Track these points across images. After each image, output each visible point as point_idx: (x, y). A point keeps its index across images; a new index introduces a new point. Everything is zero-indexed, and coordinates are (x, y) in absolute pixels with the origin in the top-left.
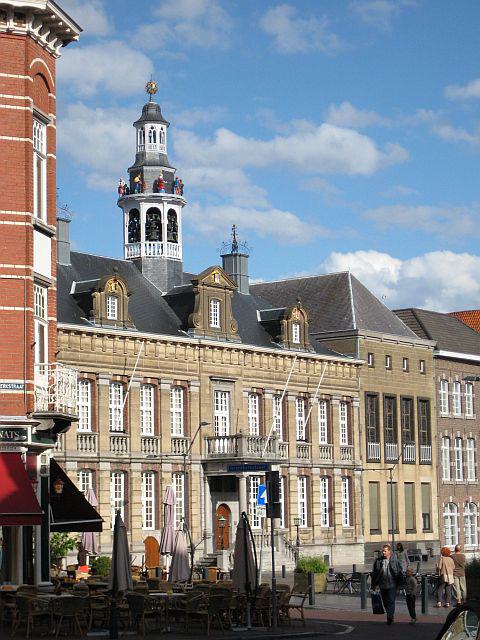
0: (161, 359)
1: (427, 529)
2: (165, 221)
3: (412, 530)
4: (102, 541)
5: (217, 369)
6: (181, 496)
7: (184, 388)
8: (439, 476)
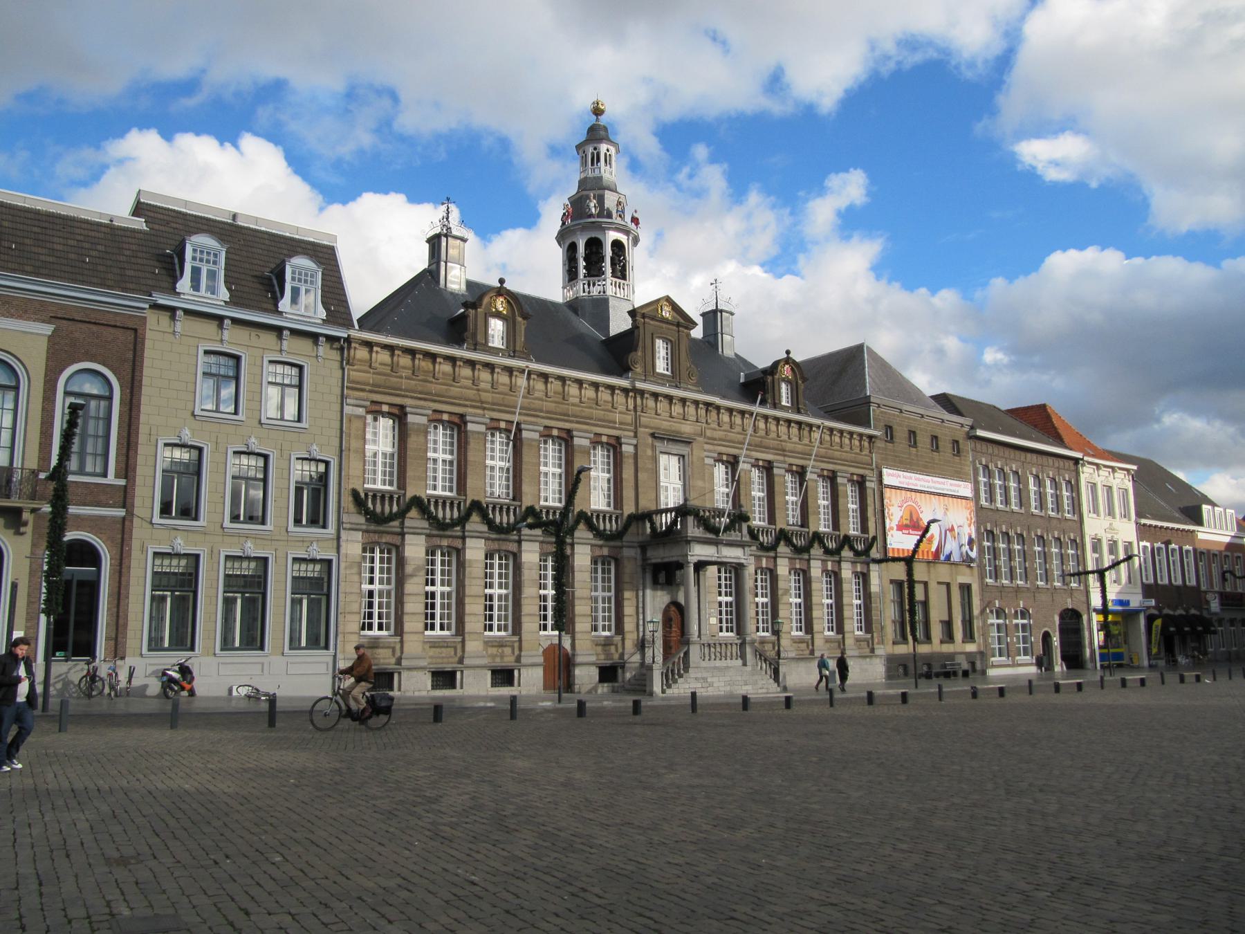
0: (573, 405)
1: (969, 636)
2: (608, 252)
3: (949, 636)
4: (467, 648)
5: (666, 425)
6: (609, 591)
7: (614, 446)
8: (982, 577)
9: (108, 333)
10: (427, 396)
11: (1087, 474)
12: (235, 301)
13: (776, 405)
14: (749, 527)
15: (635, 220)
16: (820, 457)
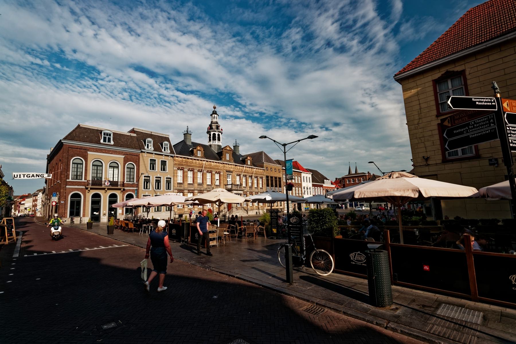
2: (217, 136)
9: (133, 156)
10: (188, 166)
11: (303, 175)
12: (154, 150)
13: (247, 165)
14: (417, 31)
15: (222, 130)
16: (255, 174)
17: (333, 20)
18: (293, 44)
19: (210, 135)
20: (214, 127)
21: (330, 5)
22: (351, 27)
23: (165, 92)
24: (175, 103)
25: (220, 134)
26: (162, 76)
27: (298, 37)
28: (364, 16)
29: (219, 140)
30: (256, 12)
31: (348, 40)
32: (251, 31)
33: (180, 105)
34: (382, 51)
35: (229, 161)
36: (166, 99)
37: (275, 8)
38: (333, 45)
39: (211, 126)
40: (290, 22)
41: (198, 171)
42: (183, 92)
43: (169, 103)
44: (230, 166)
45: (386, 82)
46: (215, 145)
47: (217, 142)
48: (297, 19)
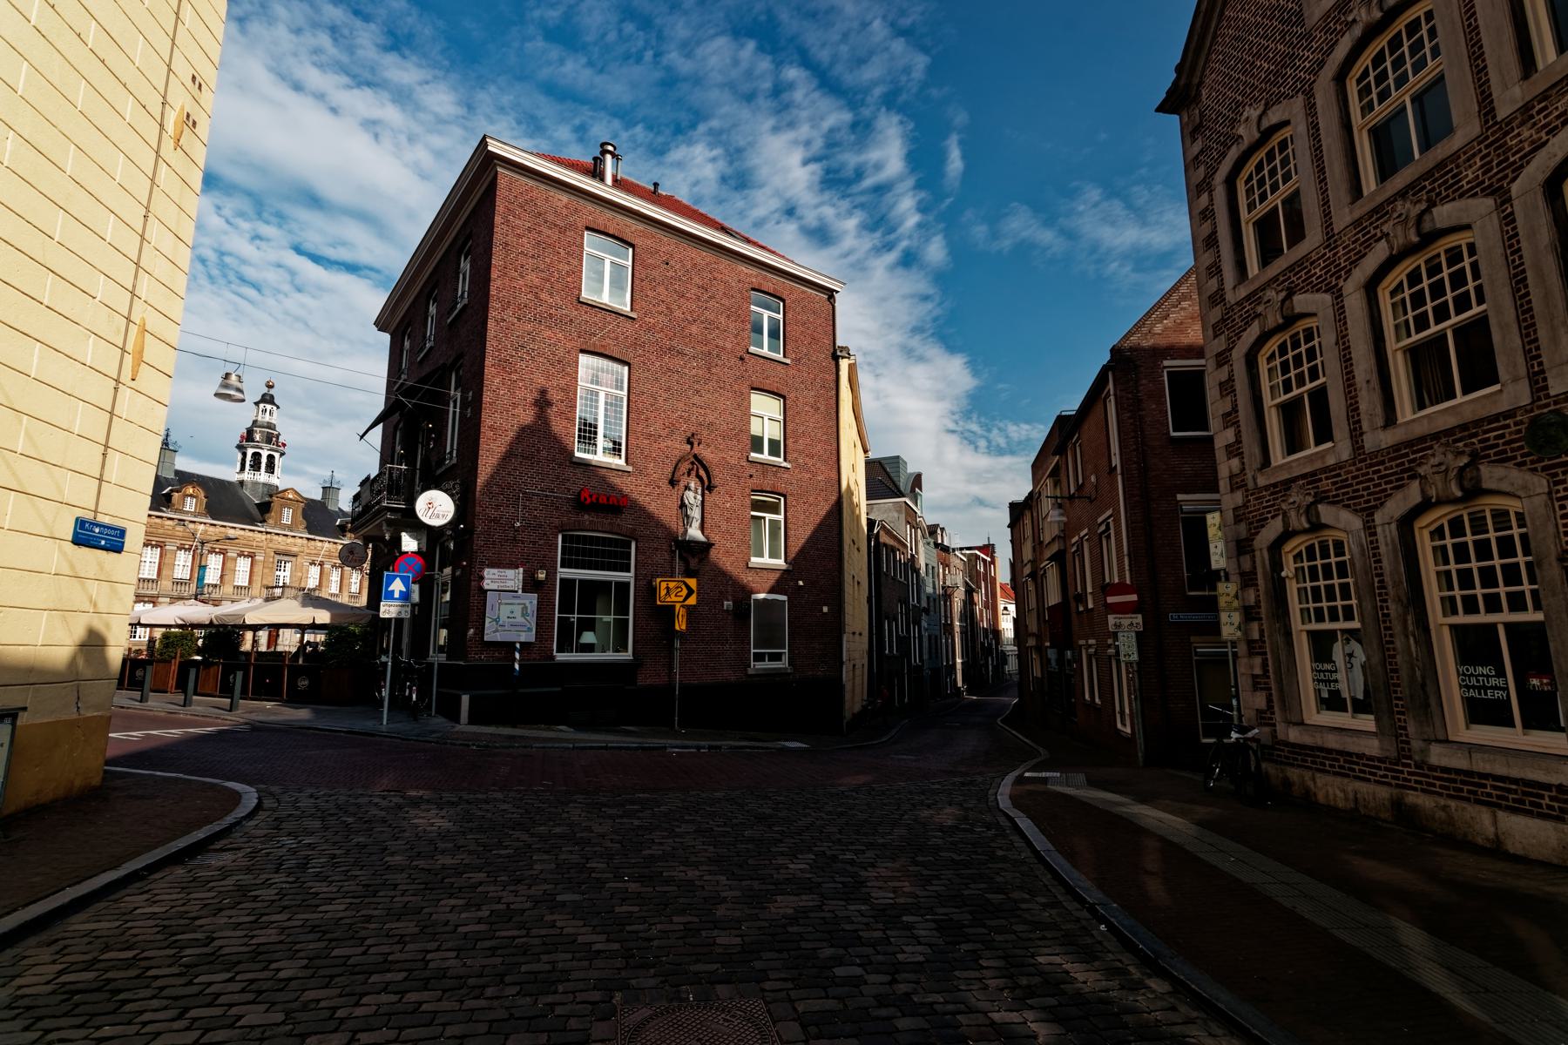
17: (809, 154)
18: (696, 189)
19: (244, 455)
20: (257, 437)
21: (804, 114)
22: (848, 182)
23: (247, 249)
24: (279, 292)
25: (277, 455)
26: (249, 194)
27: (709, 172)
28: (878, 167)
29: (271, 468)
30: (601, 71)
31: (838, 215)
32: (577, 122)
33: (294, 302)
34: (909, 260)
35: (290, 528)
36: (249, 272)
37: (658, 75)
38: (800, 218)
39: (250, 432)
40: (693, 126)
41: (180, 548)
42: (316, 259)
43: (257, 287)
44: (290, 540)
45: (915, 342)
46: (255, 484)
47: (262, 477)
48: (715, 123)
